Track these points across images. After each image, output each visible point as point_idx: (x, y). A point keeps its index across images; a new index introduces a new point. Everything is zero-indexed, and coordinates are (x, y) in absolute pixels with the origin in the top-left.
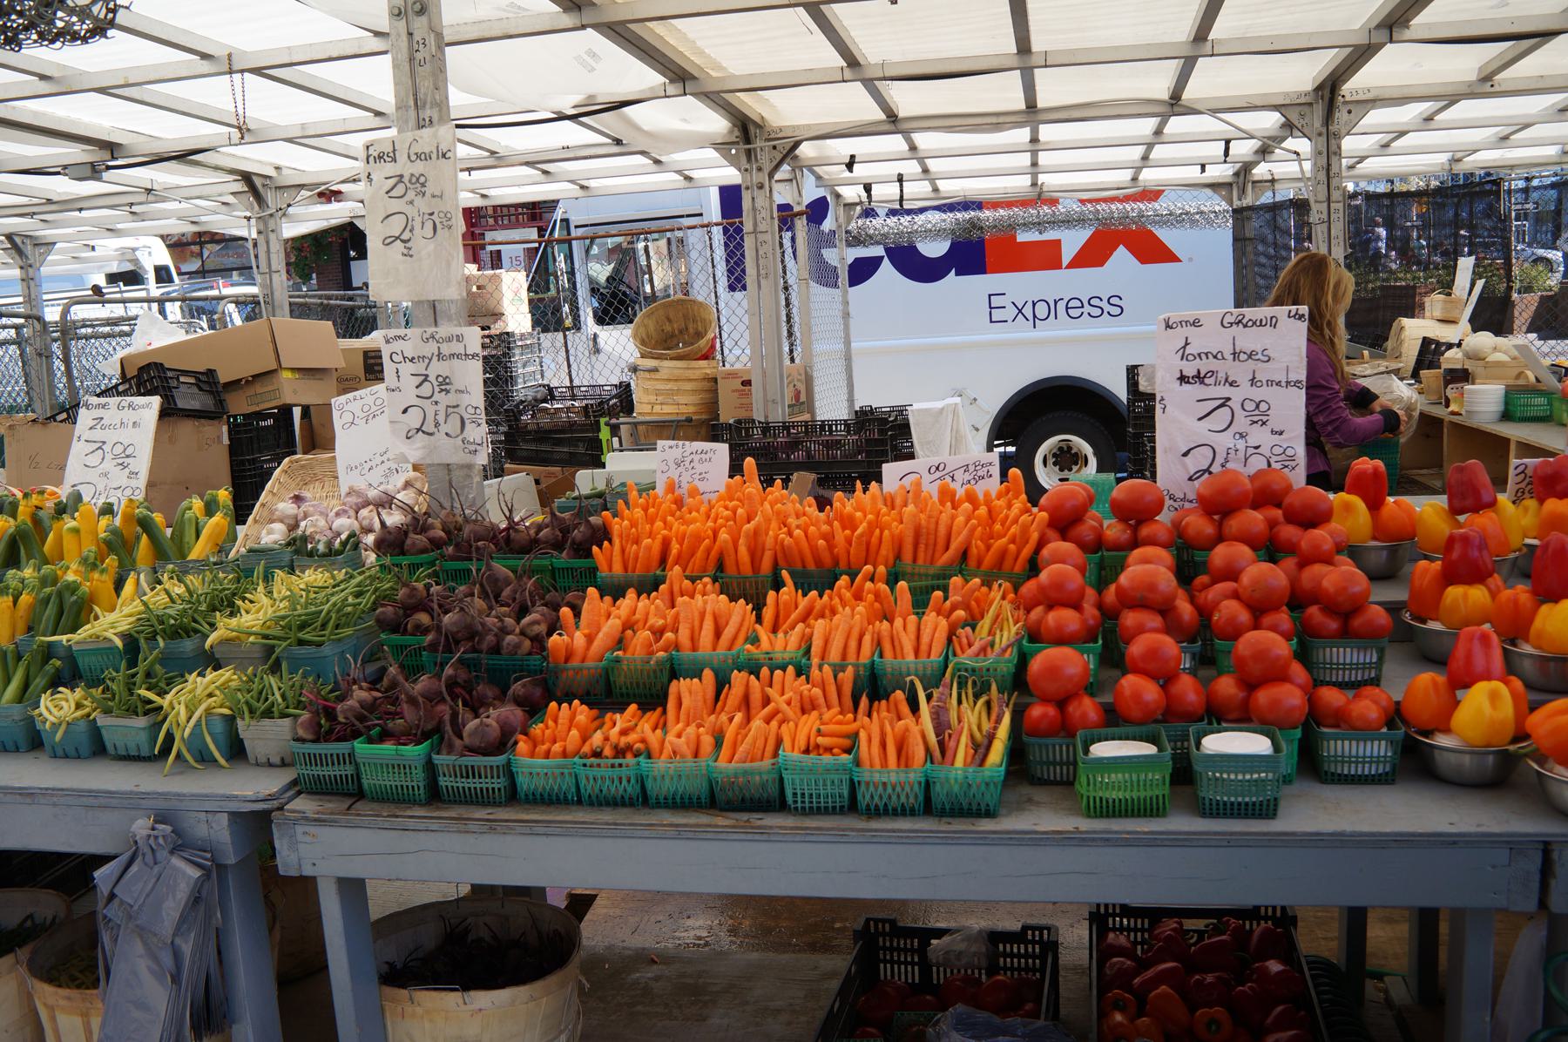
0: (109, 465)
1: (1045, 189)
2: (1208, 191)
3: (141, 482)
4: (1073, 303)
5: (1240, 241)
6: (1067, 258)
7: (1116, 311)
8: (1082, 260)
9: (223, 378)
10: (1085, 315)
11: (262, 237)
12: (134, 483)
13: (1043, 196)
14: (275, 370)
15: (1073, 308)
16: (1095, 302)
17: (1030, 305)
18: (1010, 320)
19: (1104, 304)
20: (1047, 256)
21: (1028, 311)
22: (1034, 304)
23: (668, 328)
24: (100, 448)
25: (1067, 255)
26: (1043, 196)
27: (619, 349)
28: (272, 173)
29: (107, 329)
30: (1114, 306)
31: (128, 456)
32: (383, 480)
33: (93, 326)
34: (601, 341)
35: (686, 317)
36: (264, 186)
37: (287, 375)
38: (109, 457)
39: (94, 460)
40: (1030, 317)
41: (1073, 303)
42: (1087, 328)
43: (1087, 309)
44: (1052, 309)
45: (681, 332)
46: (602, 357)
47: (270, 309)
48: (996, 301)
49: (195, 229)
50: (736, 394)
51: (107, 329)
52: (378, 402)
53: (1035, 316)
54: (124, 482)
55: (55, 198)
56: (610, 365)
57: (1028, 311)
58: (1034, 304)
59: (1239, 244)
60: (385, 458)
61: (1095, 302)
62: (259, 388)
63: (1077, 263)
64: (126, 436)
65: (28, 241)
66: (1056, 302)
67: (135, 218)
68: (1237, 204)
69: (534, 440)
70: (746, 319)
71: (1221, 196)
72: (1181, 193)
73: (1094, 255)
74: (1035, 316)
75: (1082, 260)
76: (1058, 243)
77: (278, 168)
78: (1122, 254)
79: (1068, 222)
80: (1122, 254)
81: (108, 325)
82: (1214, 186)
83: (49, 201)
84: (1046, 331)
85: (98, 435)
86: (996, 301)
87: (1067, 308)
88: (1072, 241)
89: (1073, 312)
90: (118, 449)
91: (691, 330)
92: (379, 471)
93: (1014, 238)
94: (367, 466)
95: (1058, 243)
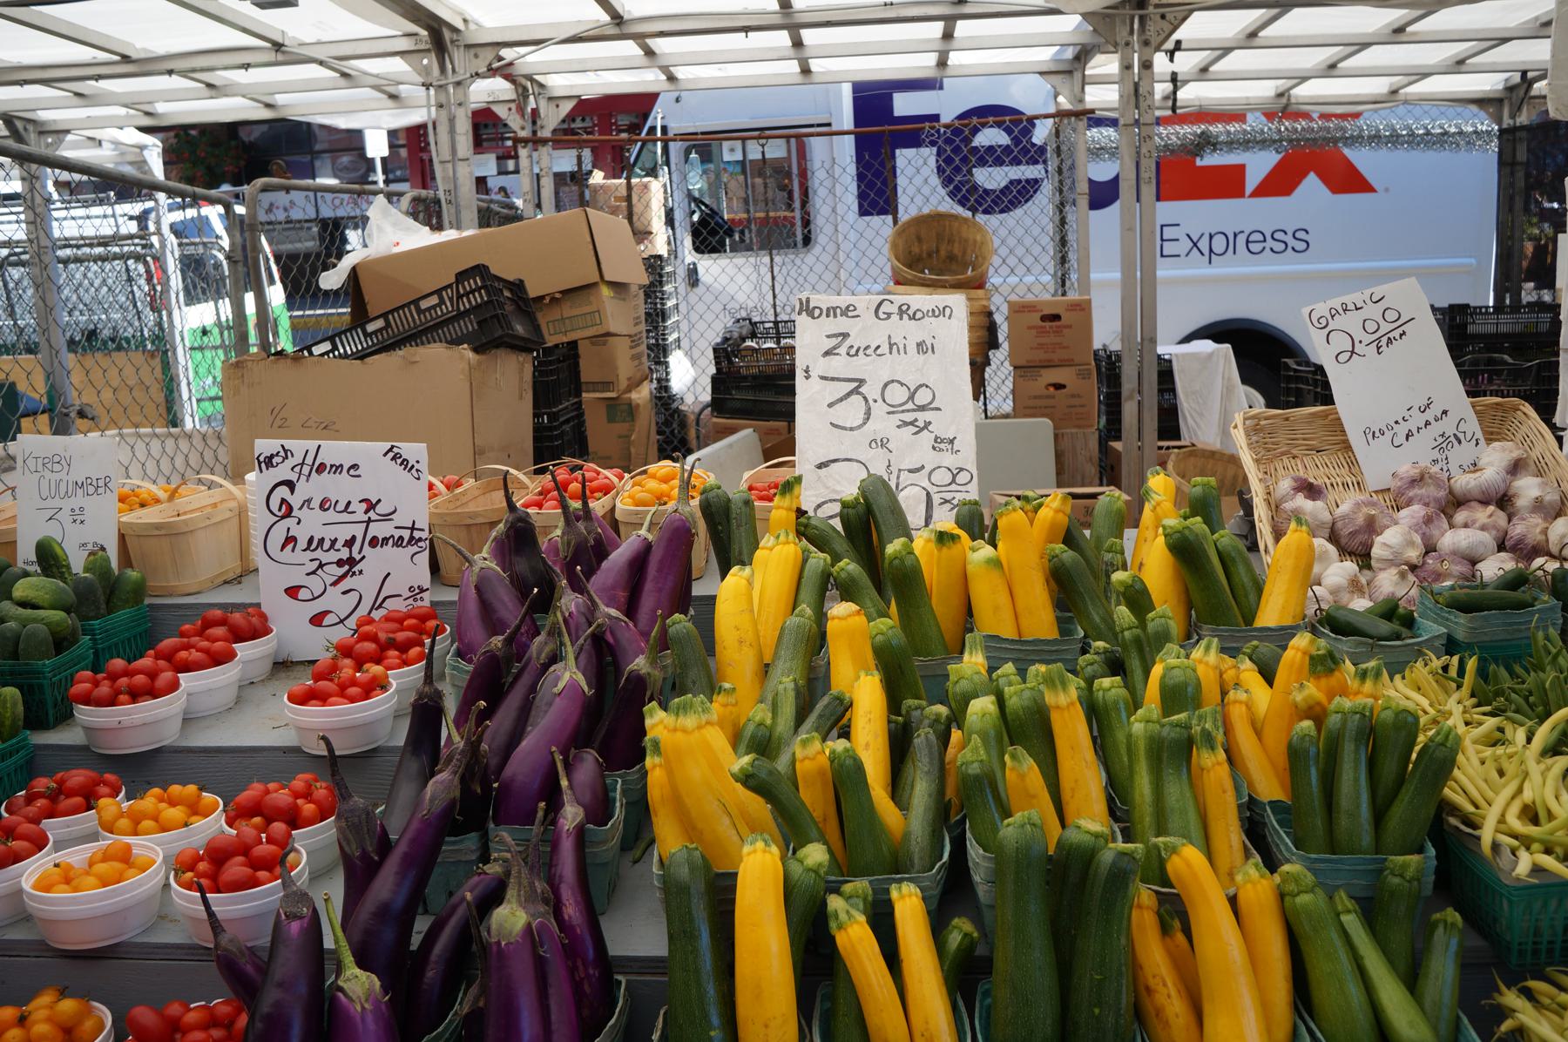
0: (883, 424)
1: (1293, 100)
2: (1474, 108)
3: (967, 454)
4: (1254, 237)
5: (1506, 163)
6: (1250, 186)
7: (1301, 246)
8: (1268, 188)
9: (533, 291)
10: (1268, 250)
11: (444, 112)
12: (949, 460)
13: (1290, 109)
14: (595, 285)
15: (1254, 242)
16: (1278, 235)
17: (1206, 238)
18: (1183, 254)
19: (1289, 239)
20: (1228, 183)
21: (1204, 245)
22: (1211, 237)
23: (916, 250)
24: (855, 391)
25: (1252, 181)
26: (1290, 109)
27: (724, 279)
28: (460, 25)
29: (99, 250)
30: (1297, 241)
31: (922, 408)
32: (1436, 454)
33: (105, 245)
34: (701, 270)
35: (939, 237)
36: (452, 42)
37: (605, 291)
38: (879, 409)
39: (852, 412)
40: (1206, 251)
41: (1254, 237)
42: (1268, 266)
43: (1270, 243)
44: (1231, 241)
45: (930, 255)
46: (700, 290)
47: (453, 211)
48: (1168, 233)
49: (266, 114)
50: (1034, 332)
51: (99, 250)
52: (1391, 316)
53: (1211, 250)
54: (929, 458)
55: (134, 55)
56: (708, 298)
57: (1204, 245)
58: (1211, 237)
59: (1507, 170)
60: (1429, 415)
61: (1278, 235)
62: (568, 310)
63: (1264, 190)
64: (909, 368)
65: (31, 127)
66: (1235, 235)
67: (213, 93)
68: (1507, 122)
69: (752, 388)
70: (997, 242)
71: (1488, 113)
72: (1443, 109)
73: (1280, 183)
74: (1211, 250)
75: (1268, 188)
76: (1241, 169)
77: (465, 21)
78: (1312, 182)
79: (1247, 143)
80: (1312, 182)
81: (100, 245)
82: (1481, 102)
83: (126, 59)
84: (1221, 268)
85: (838, 366)
86: (1168, 233)
87: (1248, 242)
88: (1259, 165)
89: (1253, 247)
90: (897, 395)
91: (943, 253)
92: (1425, 440)
93: (1194, 162)
94: (1402, 430)
95: (1241, 169)
